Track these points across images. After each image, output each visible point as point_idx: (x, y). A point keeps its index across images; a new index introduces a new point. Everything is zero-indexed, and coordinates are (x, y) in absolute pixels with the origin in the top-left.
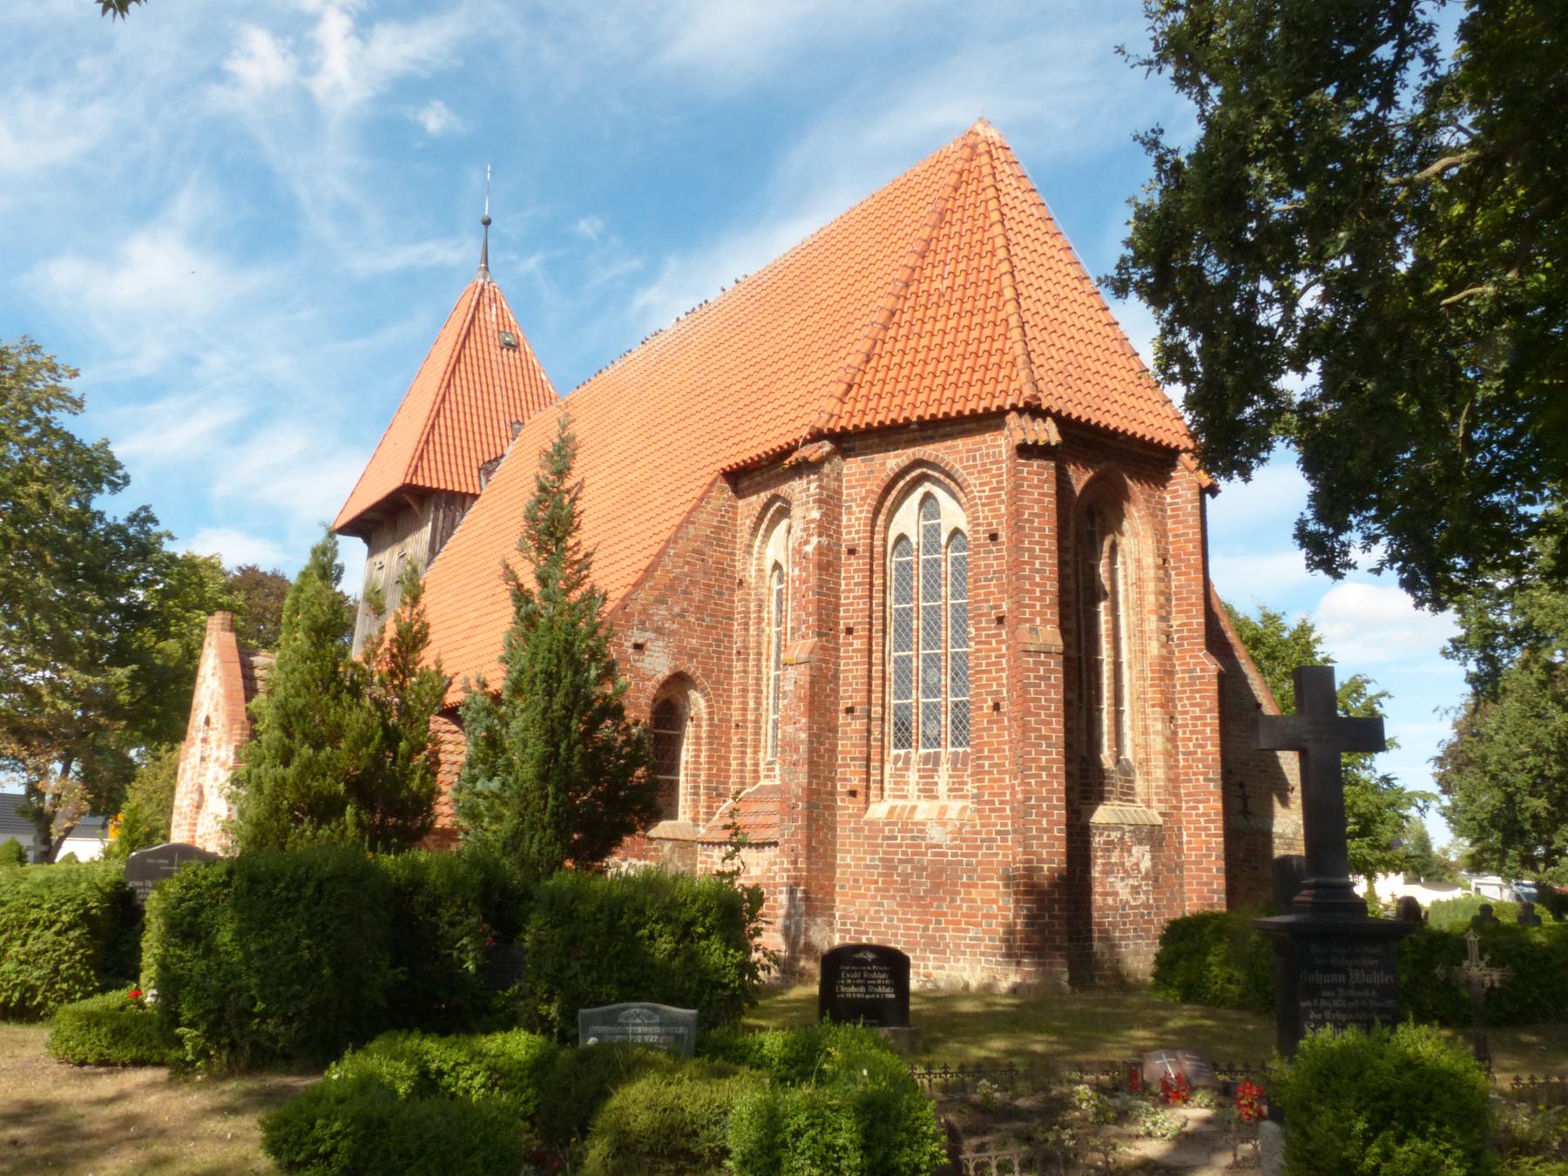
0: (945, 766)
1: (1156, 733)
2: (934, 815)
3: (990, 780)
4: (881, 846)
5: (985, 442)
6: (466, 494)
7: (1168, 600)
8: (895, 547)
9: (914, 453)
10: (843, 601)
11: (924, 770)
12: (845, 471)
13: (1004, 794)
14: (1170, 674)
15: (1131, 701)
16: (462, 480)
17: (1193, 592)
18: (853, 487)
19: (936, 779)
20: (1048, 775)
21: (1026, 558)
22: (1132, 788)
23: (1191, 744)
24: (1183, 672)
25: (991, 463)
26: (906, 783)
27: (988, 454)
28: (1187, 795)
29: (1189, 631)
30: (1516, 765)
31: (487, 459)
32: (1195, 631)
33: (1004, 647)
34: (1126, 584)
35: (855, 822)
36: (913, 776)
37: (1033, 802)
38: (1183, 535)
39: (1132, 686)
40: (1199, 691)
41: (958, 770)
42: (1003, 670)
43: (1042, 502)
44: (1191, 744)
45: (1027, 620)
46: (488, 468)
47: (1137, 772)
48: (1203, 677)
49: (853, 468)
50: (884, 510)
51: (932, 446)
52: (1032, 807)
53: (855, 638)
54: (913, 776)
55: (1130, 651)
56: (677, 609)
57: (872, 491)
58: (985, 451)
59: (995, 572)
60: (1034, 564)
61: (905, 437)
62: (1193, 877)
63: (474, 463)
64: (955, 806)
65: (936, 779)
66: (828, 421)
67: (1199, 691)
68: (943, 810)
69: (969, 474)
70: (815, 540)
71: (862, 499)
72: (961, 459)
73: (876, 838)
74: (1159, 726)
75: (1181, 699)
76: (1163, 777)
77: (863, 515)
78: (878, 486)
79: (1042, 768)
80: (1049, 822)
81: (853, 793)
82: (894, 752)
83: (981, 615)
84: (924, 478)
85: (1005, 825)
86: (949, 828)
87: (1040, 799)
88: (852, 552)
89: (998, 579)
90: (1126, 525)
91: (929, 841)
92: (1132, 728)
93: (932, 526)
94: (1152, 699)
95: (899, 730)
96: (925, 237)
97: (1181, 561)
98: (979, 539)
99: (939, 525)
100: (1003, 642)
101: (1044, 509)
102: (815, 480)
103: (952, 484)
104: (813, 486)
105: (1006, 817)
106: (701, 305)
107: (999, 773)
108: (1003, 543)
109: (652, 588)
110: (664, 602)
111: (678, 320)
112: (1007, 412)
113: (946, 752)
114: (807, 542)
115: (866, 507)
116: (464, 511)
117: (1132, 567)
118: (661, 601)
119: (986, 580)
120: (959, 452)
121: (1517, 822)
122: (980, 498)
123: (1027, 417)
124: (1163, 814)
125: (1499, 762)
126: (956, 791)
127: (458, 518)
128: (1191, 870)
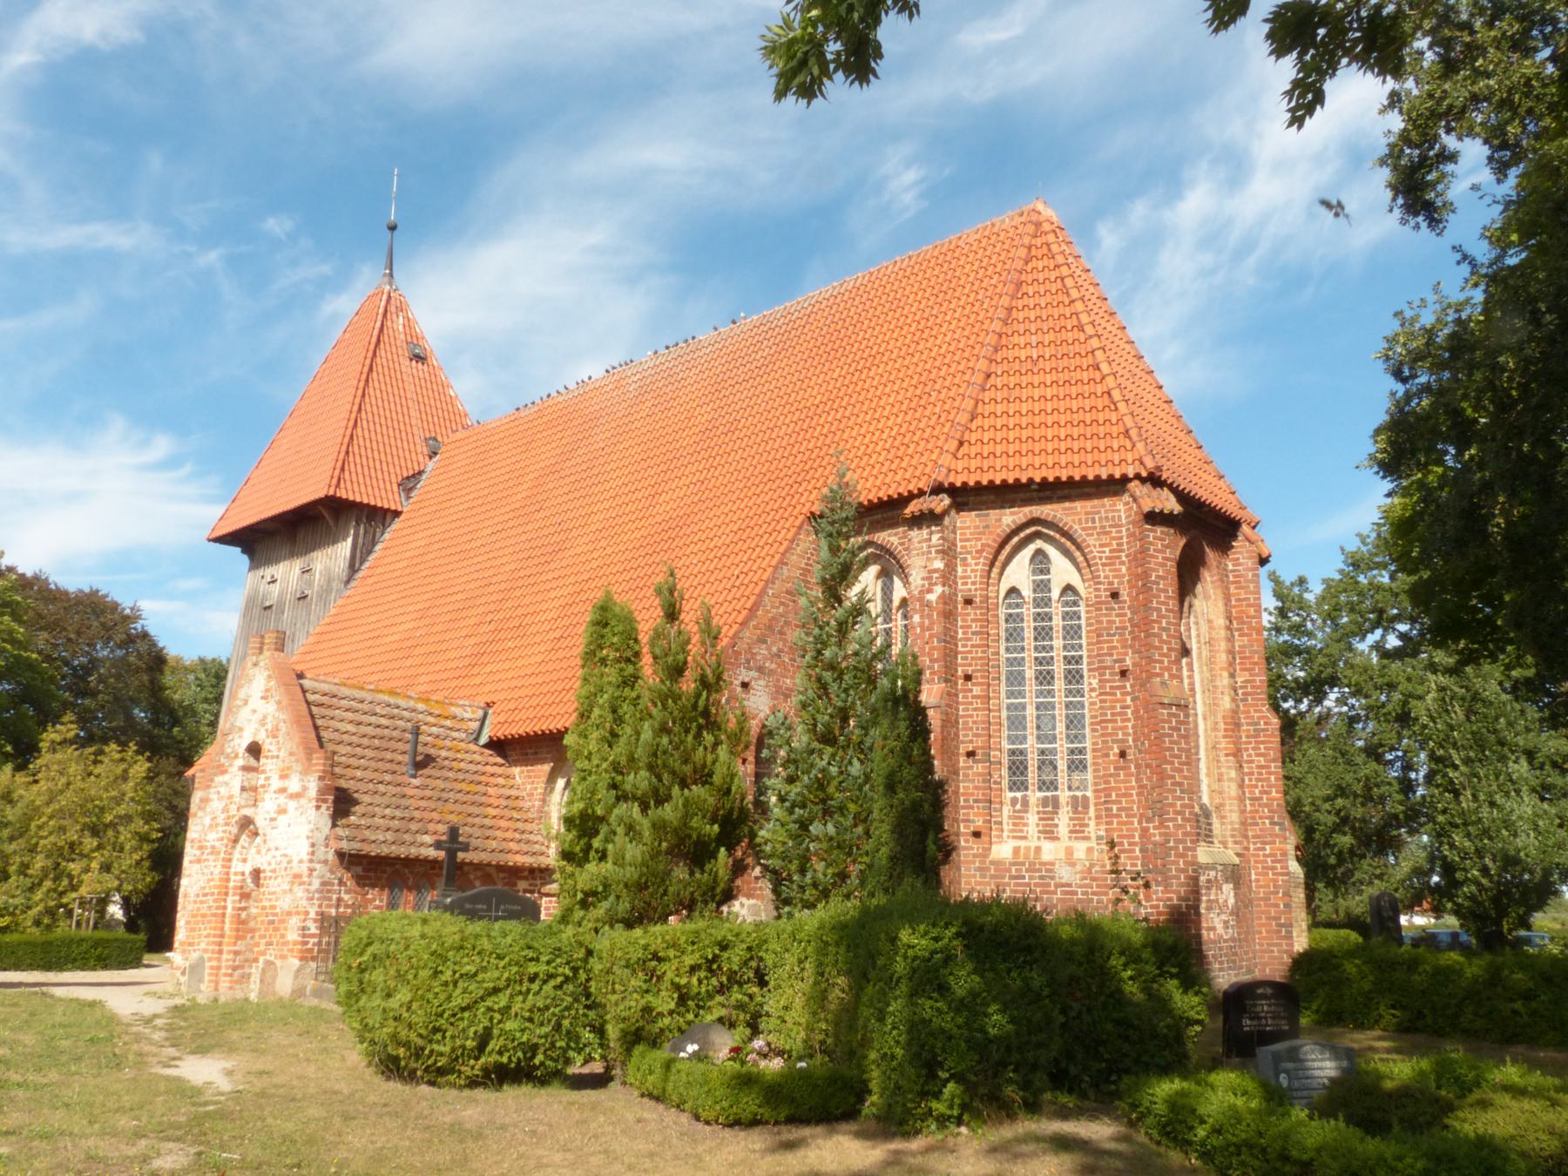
0: (1065, 809)
1: (1230, 780)
2: (1062, 855)
3: (1119, 823)
4: (1009, 885)
5: (1103, 506)
6: (388, 510)
7: (1234, 658)
8: (1005, 598)
9: (1031, 512)
10: (960, 649)
11: (1044, 813)
12: (958, 524)
13: (1133, 836)
14: (1238, 725)
15: (1206, 750)
16: (363, 490)
17: (1256, 652)
18: (968, 540)
19: (1056, 821)
20: (1183, 819)
21: (1155, 617)
22: (1211, 831)
23: (1257, 791)
24: (1248, 724)
25: (1110, 526)
26: (1026, 825)
27: (1107, 518)
28: (1254, 837)
29: (1253, 687)
30: (1327, 806)
31: (405, 475)
32: (1258, 687)
33: (1129, 698)
34: (1199, 642)
35: (980, 862)
36: (1032, 818)
37: (1172, 844)
38: (1245, 599)
39: (1206, 737)
40: (1262, 742)
41: (1080, 813)
42: (1129, 720)
43: (1165, 565)
44: (1257, 791)
45: (1157, 675)
46: (409, 483)
47: (1214, 815)
48: (1267, 730)
49: (967, 523)
50: (998, 564)
51: (1049, 507)
52: (1171, 849)
53: (974, 684)
54: (1032, 818)
55: (1204, 703)
56: (774, 649)
57: (989, 546)
58: (1103, 515)
59: (1117, 628)
60: (1161, 623)
61: (1022, 495)
62: (1262, 912)
63: (394, 480)
64: (1080, 849)
65: (1056, 821)
66: (947, 475)
67: (1262, 742)
68: (1069, 852)
69: (1088, 535)
70: (939, 589)
71: (977, 552)
72: (1080, 520)
73: (1004, 877)
74: (1233, 774)
75: (1247, 749)
76: (1237, 820)
77: (980, 567)
78: (994, 540)
79: (1177, 813)
80: (1185, 863)
81: (977, 834)
82: (1010, 795)
83: (1106, 668)
84: (1038, 535)
85: (1136, 865)
86: (1079, 868)
87: (1177, 841)
88: (968, 602)
89: (1120, 635)
90: (1199, 588)
91: (1057, 880)
92: (1208, 775)
93: (1042, 581)
94: (1226, 749)
95: (1014, 773)
96: (1006, 305)
97: (1243, 623)
98: (1100, 596)
99: (1049, 580)
100: (1127, 694)
101: (1168, 572)
102: (938, 532)
103: (1068, 544)
104: (935, 538)
105: (1137, 858)
106: (686, 341)
107: (1127, 816)
108: (1125, 602)
109: (756, 627)
110: (765, 642)
111: (656, 352)
112: (1130, 480)
113: (1035, 796)
114: (930, 591)
115: (982, 560)
116: (385, 527)
117: (1204, 628)
118: (762, 640)
119: (1109, 635)
120: (1078, 514)
121: (1320, 857)
122: (1101, 558)
123: (1148, 485)
124: (1238, 855)
125: (1313, 804)
126: (1078, 832)
127: (378, 534)
128: (1259, 905)
